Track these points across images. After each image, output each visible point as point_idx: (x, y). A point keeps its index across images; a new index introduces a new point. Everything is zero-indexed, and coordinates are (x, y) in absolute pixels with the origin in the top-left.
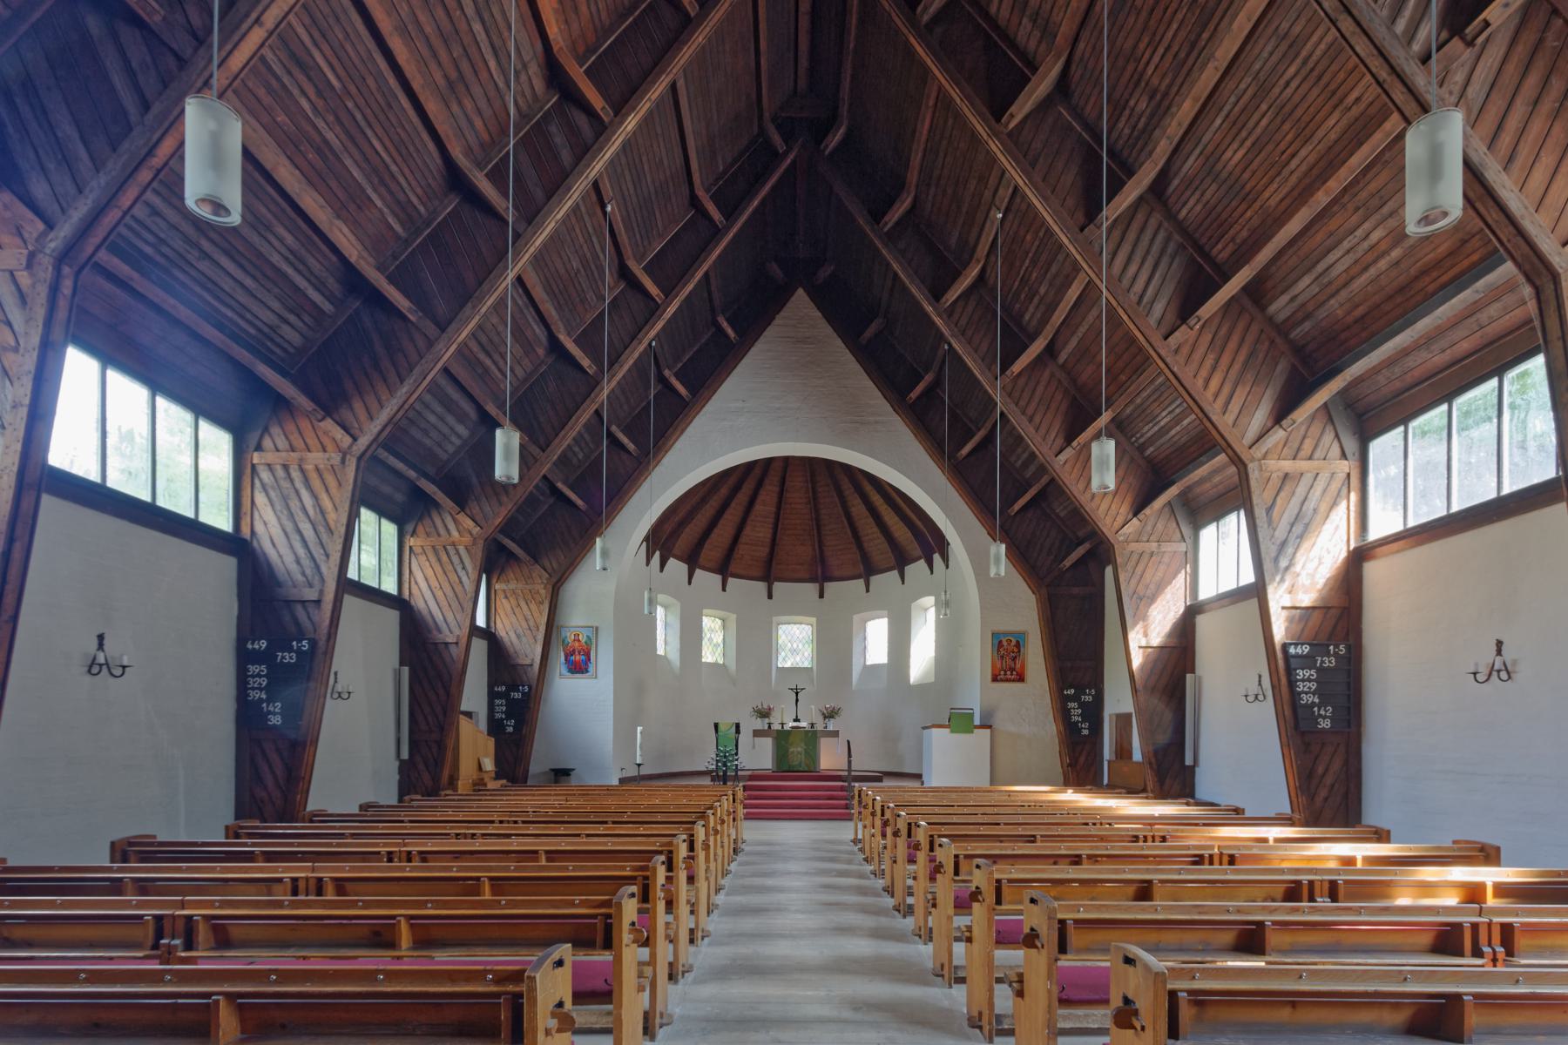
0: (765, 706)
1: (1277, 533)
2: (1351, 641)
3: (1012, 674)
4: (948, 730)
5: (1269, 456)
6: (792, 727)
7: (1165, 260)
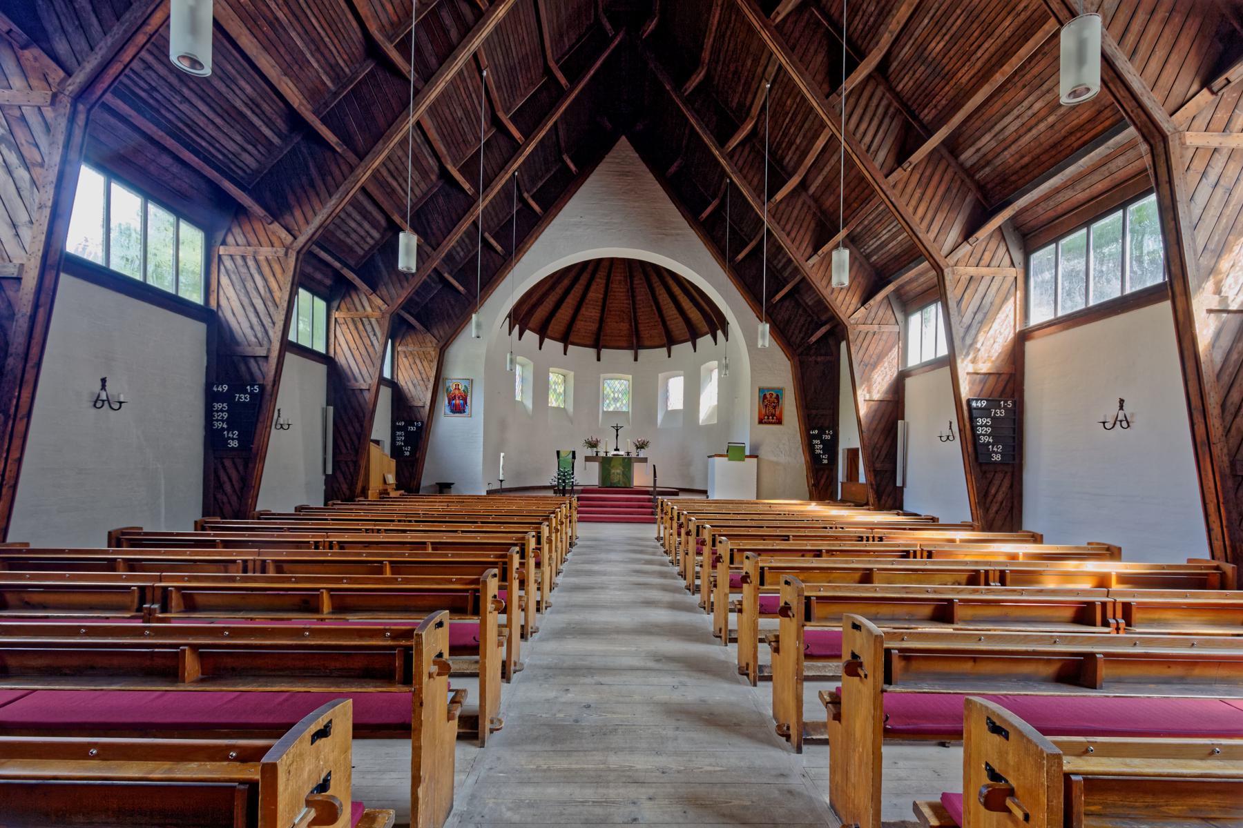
0: (594, 439)
2: (1016, 398)
5: (959, 264)
6: (614, 455)
7: (887, 121)
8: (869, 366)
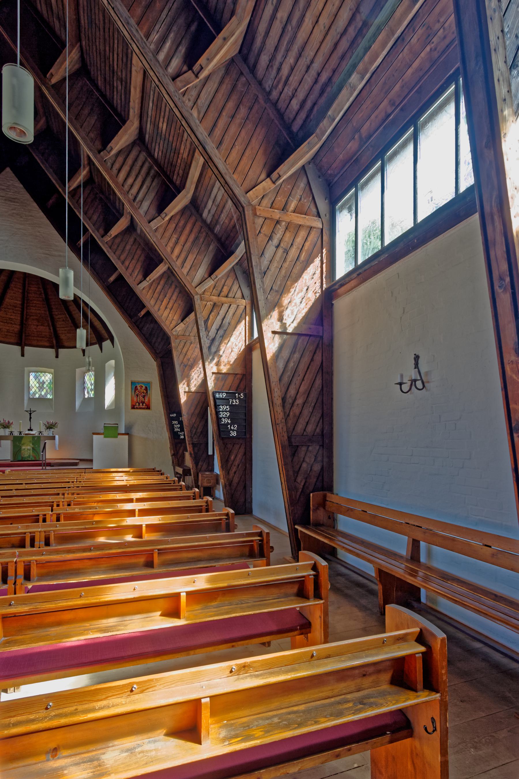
0: (7, 422)
1: (210, 334)
2: (247, 391)
3: (143, 405)
4: (102, 436)
5: (206, 293)
6: (26, 434)
7: (149, 180)
8: (188, 366)
